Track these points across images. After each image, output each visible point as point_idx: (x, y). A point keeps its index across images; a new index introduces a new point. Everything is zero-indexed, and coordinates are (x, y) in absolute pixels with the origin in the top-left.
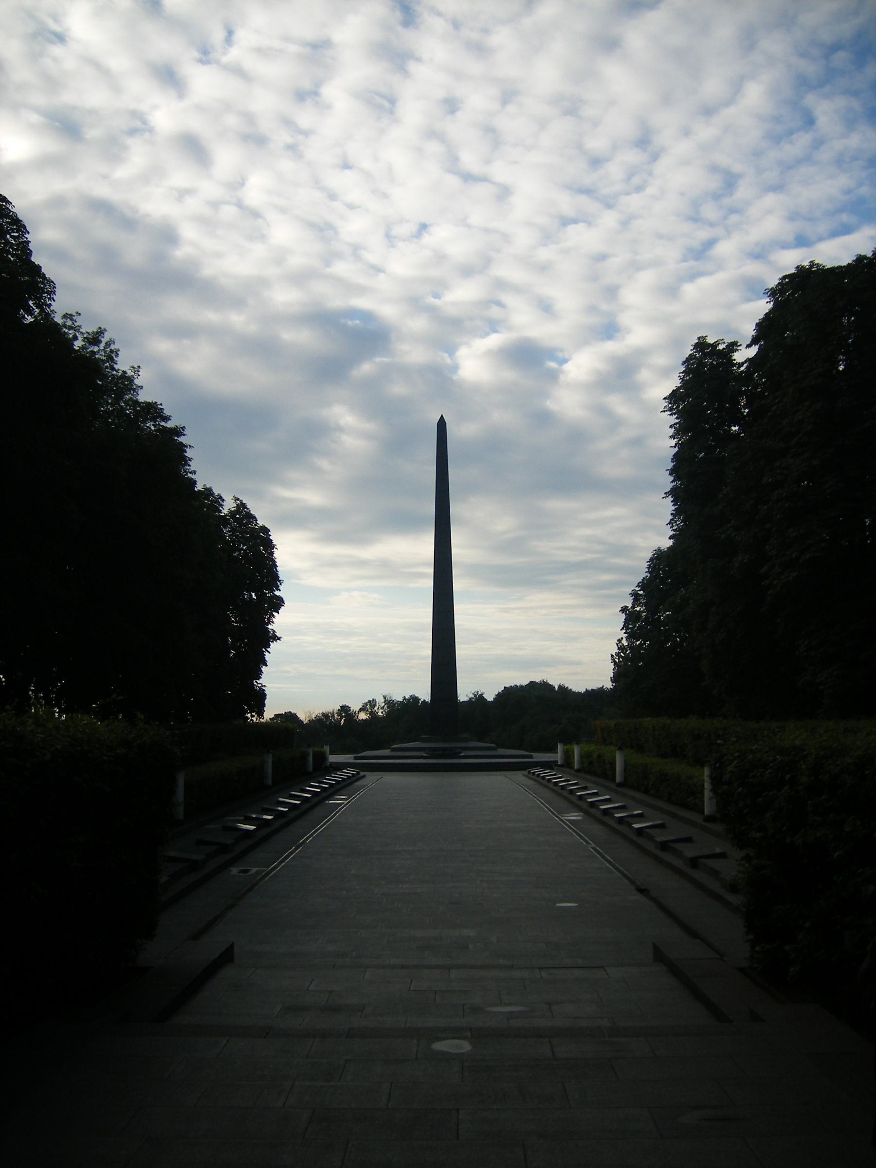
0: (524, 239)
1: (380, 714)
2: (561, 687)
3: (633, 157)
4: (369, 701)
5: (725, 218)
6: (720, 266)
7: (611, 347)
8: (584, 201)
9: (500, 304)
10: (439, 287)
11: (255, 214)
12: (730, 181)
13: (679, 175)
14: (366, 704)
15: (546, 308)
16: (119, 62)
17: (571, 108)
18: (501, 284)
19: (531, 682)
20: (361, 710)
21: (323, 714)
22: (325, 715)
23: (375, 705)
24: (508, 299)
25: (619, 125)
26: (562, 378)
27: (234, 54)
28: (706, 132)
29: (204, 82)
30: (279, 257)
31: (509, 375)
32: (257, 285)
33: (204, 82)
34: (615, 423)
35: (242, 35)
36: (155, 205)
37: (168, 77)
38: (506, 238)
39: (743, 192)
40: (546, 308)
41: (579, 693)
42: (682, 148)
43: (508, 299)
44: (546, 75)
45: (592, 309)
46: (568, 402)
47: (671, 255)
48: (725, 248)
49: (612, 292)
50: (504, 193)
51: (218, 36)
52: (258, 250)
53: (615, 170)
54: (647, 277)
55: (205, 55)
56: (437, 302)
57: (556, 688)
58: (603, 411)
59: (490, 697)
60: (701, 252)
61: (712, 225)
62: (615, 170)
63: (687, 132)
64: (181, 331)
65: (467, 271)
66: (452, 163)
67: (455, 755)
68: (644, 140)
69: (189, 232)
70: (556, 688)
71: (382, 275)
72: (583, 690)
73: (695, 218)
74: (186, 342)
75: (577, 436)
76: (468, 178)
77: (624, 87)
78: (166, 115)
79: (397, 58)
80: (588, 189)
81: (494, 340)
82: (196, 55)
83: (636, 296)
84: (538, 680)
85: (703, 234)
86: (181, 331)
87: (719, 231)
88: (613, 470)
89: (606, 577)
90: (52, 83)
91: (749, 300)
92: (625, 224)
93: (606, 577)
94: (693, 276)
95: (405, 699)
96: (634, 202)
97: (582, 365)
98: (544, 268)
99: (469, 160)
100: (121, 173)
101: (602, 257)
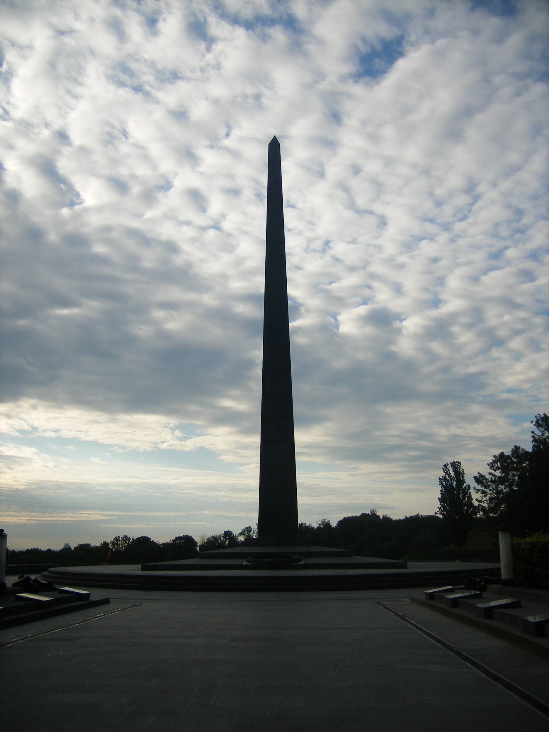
0: (390, 249)
1: (254, 537)
2: (385, 518)
3: (462, 200)
4: (247, 528)
5: (513, 236)
6: (509, 263)
7: (434, 313)
8: (428, 226)
9: (369, 287)
10: (334, 279)
11: (229, 235)
12: (519, 213)
13: (490, 211)
14: (244, 530)
15: (398, 290)
16: (156, 150)
17: (427, 172)
18: (373, 276)
19: (363, 514)
20: (241, 534)
21: (213, 537)
22: (214, 538)
23: (251, 531)
24: (376, 285)
25: (455, 181)
26: (404, 331)
27: (227, 142)
28: (505, 186)
29: (210, 159)
30: (239, 262)
31: (369, 330)
32: (224, 277)
33: (210, 159)
34: (433, 358)
35: (236, 133)
36: (167, 231)
37: (188, 155)
38: (379, 248)
39: (527, 220)
40: (398, 290)
41: (400, 521)
42: (493, 194)
43: (376, 285)
44: (413, 153)
45: (426, 290)
46: (405, 346)
47: (479, 257)
48: (511, 253)
49: (441, 281)
50: (383, 222)
51: (223, 131)
52: (226, 258)
53: (448, 210)
54: (460, 271)
55: (214, 144)
56: (329, 287)
57: (381, 518)
58: (427, 351)
59: (334, 524)
60: (497, 255)
61: (504, 239)
62: (448, 210)
63: (494, 185)
64: (170, 306)
65: (352, 269)
66: (352, 206)
67: (291, 564)
68: (471, 189)
69: (186, 247)
70: (381, 518)
71: (300, 271)
72: (402, 518)
73: (495, 235)
74: (173, 312)
75: (409, 366)
76: (360, 212)
77: (461, 161)
78: (184, 178)
79: (330, 144)
80: (438, 219)
81: (362, 310)
82: (208, 143)
83: (454, 282)
84: (354, 515)
85: (499, 245)
86: (170, 306)
87: (508, 243)
88: (427, 387)
89: (413, 453)
90: (114, 162)
91: (524, 283)
92: (452, 241)
93: (413, 453)
94: (492, 269)
95: (453, 490)
96: (459, 226)
97: (412, 324)
98: (401, 266)
99: (361, 202)
100: (149, 215)
101: (435, 260)
